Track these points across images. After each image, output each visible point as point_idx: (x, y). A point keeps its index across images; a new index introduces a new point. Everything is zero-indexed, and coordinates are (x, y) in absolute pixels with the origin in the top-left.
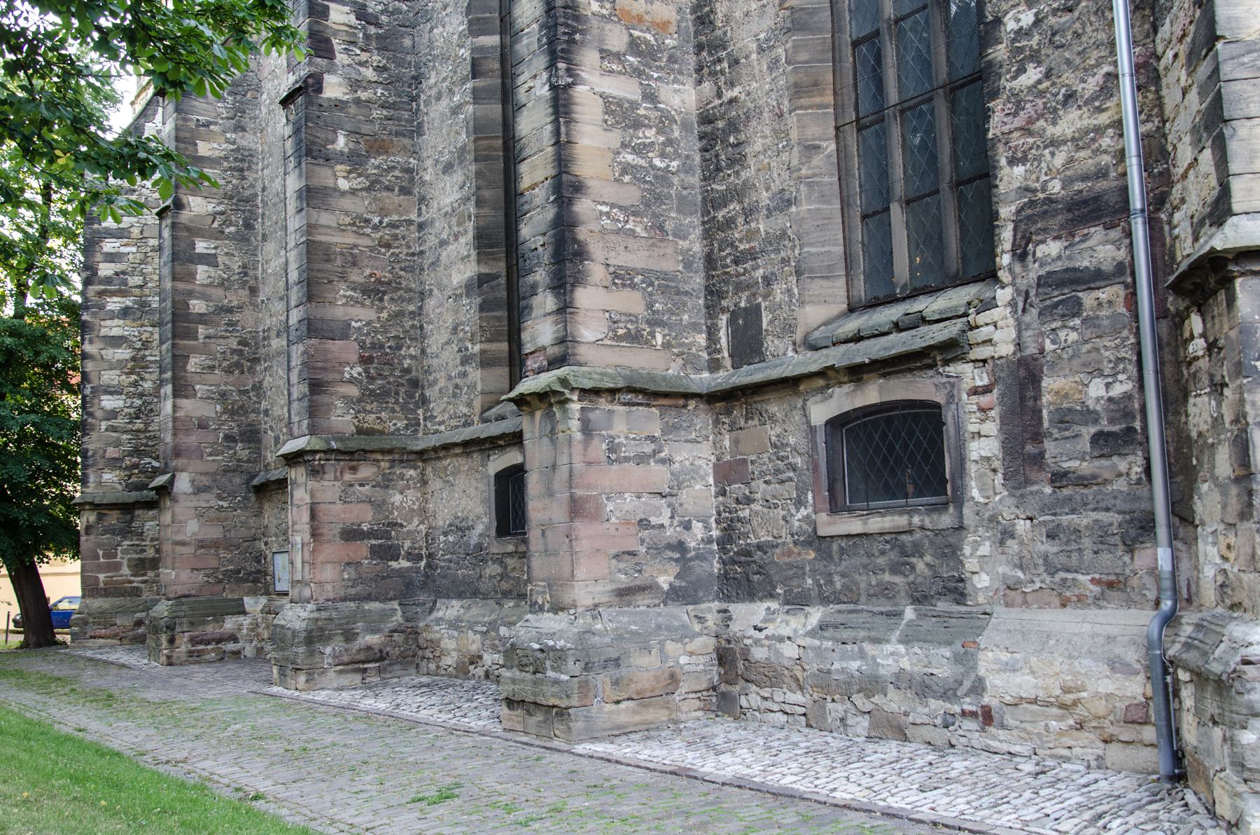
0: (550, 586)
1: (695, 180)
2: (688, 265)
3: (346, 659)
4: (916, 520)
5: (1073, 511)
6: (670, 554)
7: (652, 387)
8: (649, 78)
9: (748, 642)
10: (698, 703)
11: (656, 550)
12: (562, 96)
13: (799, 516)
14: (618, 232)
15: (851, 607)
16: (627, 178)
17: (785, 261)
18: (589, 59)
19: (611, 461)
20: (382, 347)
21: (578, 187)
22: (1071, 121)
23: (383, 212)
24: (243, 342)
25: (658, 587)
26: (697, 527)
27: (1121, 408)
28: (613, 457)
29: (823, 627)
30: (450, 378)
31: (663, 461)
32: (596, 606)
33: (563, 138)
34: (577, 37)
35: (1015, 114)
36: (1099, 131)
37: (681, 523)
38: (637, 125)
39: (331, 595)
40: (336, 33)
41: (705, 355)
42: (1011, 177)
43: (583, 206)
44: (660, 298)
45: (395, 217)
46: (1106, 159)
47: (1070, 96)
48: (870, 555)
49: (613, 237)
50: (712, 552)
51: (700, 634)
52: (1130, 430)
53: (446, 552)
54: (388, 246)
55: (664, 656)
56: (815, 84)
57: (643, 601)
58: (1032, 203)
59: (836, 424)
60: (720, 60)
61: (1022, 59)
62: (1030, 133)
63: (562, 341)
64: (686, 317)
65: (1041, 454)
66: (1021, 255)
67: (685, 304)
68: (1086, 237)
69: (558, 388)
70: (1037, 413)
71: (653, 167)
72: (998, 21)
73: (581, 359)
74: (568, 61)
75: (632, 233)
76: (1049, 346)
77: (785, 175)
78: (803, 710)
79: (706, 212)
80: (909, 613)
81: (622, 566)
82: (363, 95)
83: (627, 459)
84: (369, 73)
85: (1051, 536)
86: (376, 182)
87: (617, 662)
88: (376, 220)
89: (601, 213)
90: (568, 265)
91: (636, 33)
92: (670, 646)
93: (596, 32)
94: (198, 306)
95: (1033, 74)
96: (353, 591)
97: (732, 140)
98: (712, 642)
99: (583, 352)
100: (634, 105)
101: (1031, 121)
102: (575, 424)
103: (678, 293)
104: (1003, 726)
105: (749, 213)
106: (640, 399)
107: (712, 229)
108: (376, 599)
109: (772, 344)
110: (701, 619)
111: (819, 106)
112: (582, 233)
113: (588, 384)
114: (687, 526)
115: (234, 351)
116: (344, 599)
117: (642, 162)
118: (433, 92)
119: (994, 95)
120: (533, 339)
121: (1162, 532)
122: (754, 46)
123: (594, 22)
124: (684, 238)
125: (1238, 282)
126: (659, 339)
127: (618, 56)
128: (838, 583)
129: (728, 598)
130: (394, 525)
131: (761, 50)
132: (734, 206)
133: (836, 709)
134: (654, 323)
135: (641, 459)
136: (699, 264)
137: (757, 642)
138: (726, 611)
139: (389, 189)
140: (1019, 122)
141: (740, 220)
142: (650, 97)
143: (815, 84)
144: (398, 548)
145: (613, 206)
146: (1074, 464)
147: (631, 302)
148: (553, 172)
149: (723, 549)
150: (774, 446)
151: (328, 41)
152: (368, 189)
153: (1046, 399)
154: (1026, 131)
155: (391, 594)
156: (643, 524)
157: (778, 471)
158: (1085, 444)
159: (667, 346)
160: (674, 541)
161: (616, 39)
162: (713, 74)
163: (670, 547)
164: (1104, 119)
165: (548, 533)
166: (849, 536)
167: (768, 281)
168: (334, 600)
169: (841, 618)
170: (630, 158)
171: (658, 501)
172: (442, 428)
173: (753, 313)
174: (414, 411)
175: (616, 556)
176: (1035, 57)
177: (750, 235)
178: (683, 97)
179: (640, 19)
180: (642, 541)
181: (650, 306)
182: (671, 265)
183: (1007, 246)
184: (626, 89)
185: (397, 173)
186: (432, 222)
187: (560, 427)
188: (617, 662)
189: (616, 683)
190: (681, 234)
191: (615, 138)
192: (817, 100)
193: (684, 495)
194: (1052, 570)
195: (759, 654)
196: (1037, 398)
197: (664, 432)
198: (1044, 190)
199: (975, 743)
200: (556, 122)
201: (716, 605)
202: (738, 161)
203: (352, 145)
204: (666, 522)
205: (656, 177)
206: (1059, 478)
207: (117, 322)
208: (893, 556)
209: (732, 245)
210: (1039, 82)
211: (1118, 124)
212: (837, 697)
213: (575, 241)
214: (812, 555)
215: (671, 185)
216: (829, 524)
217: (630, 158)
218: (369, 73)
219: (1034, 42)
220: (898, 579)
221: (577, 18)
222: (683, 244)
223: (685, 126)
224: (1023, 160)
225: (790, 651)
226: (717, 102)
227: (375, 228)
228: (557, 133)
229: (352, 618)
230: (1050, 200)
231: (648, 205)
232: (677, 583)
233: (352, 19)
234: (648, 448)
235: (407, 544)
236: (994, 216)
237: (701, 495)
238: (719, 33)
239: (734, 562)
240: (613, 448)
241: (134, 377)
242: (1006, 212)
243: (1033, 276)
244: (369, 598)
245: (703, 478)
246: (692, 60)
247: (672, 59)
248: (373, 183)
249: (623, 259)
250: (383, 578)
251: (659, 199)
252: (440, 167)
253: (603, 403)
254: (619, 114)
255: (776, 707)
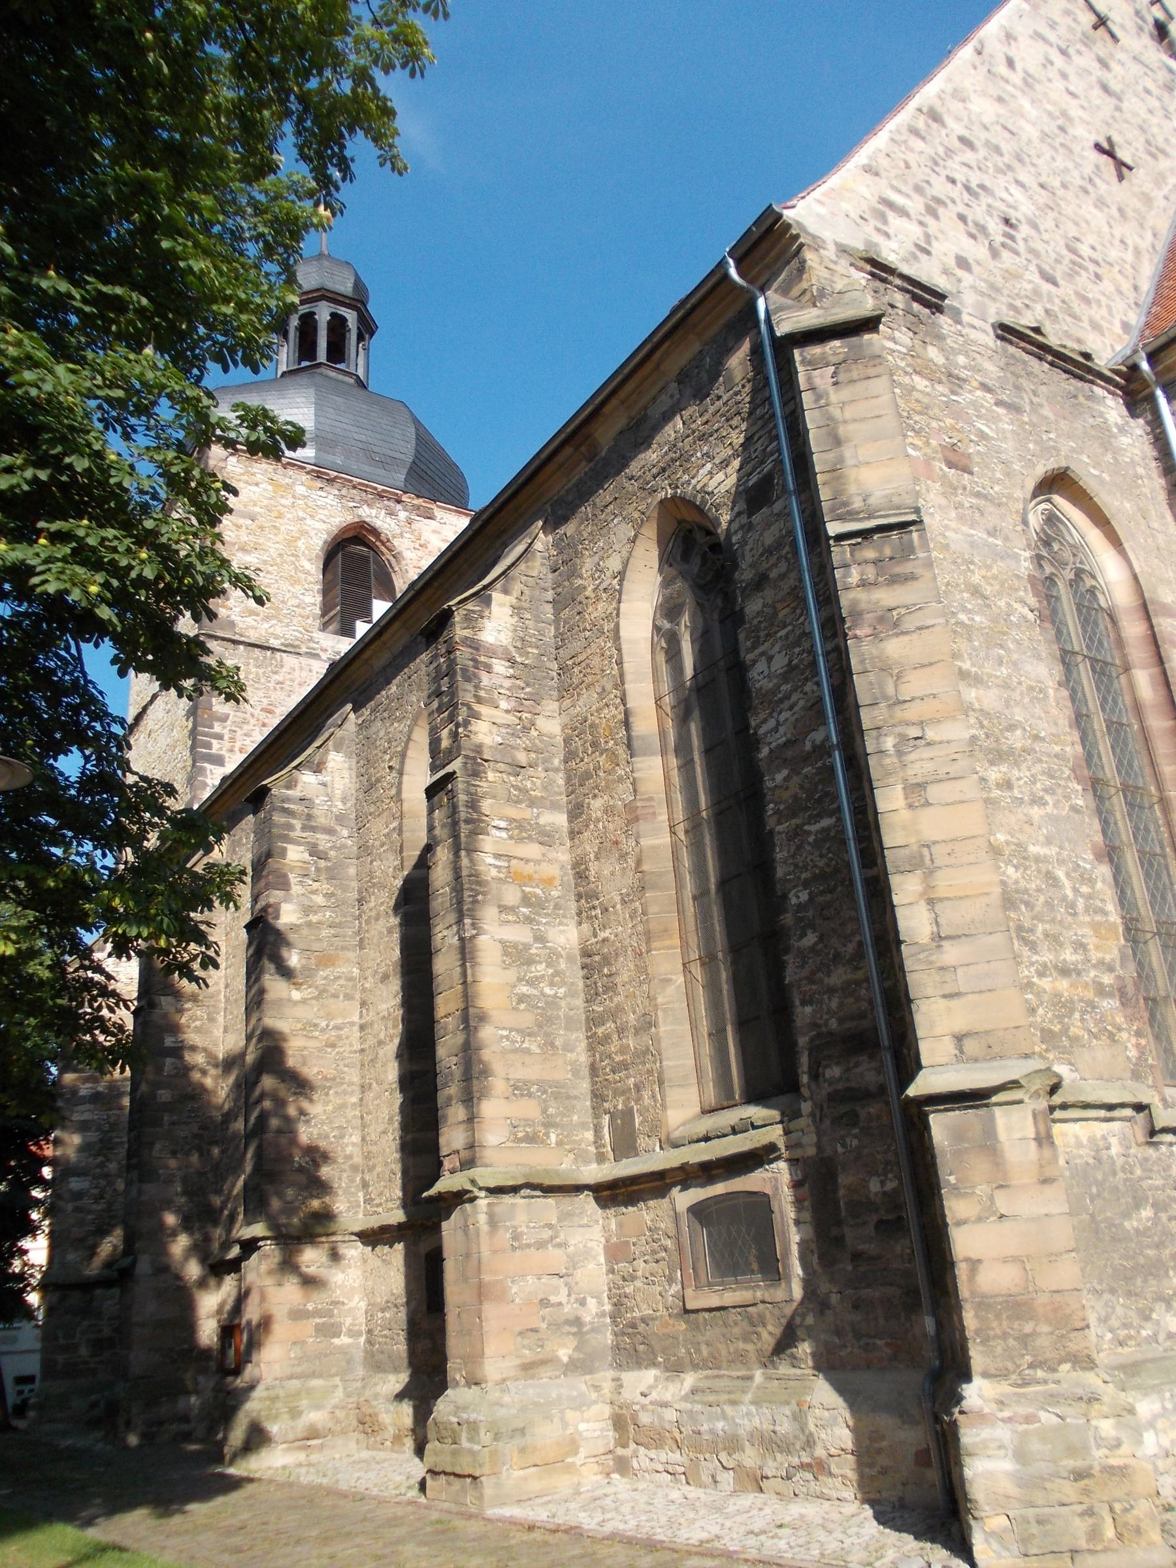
0: (465, 1364)
1: (579, 1002)
2: (576, 1073)
3: (291, 1437)
4: (759, 1294)
5: (868, 1286)
6: (567, 1328)
7: (547, 1182)
8: (538, 923)
9: (636, 1407)
10: (596, 1467)
11: (555, 1326)
12: (468, 945)
13: (672, 1292)
14: (516, 1051)
15: (715, 1372)
16: (522, 1006)
17: (650, 1072)
18: (489, 915)
19: (514, 1248)
20: (327, 1137)
21: (483, 1018)
22: (838, 976)
23: (329, 1016)
24: (203, 1127)
25: (558, 1359)
26: (592, 1303)
27: (892, 1199)
28: (516, 1244)
29: (693, 1392)
30: (386, 1164)
31: (559, 1245)
32: (504, 1380)
33: (469, 979)
34: (480, 897)
35: (802, 967)
36: (858, 983)
37: (577, 1300)
38: (530, 962)
39: (279, 1375)
40: (292, 869)
41: (592, 1149)
42: (804, 1013)
43: (486, 1033)
44: (552, 1103)
45: (340, 1021)
46: (864, 1005)
47: (837, 957)
48: (726, 1325)
49: (512, 1056)
50: (605, 1325)
51: (595, 1402)
52: (900, 1218)
53: (383, 1328)
54: (333, 1046)
55: (565, 1424)
56: (666, 931)
57: (545, 1373)
58: (819, 1035)
59: (697, 1211)
60: (594, 908)
61: (805, 926)
62: (813, 982)
63: (471, 1146)
64: (575, 1118)
65: (843, 1237)
66: (815, 1076)
67: (574, 1107)
68: (857, 1065)
69: (468, 1187)
70: (836, 1202)
71: (544, 995)
72: (785, 897)
73: (486, 1161)
74: (473, 918)
75: (527, 1051)
76: (840, 1149)
77: (647, 1002)
78: (682, 1469)
79: (589, 1029)
80: (758, 1375)
81: (526, 1342)
82: (314, 918)
83: (529, 1246)
84: (319, 900)
85: (856, 1307)
86: (325, 991)
87: (522, 1431)
88: (324, 1024)
89: (502, 1037)
90: (475, 1082)
91: (527, 889)
92: (570, 1415)
93: (494, 892)
94: (164, 1095)
95: (810, 939)
96: (298, 1370)
97: (606, 971)
98: (607, 1410)
99: (488, 1155)
100: (527, 947)
101: (813, 973)
102: (482, 1218)
103: (568, 1097)
104: (831, 1474)
105: (621, 1031)
106: (538, 1193)
107: (595, 1043)
108: (320, 1376)
109: (642, 1142)
110: (597, 1388)
111: (670, 948)
112: (486, 1054)
113: (492, 1184)
114: (583, 1303)
115: (196, 1136)
116: (291, 1377)
117: (535, 992)
118: (373, 914)
119: (787, 951)
120: (448, 1144)
121: (925, 1301)
122: (618, 899)
123: (494, 885)
124: (572, 1051)
125: (931, 1117)
126: (553, 1137)
127: (512, 909)
128: (705, 1351)
129: (620, 1367)
130: (336, 1303)
131: (624, 902)
132: (610, 1025)
133: (709, 1466)
134: (548, 1125)
135: (541, 1245)
136: (585, 1072)
137: (643, 1407)
138: (618, 1379)
139: (335, 996)
140: (805, 972)
141: (615, 1036)
142: (540, 938)
143: (666, 931)
144: (340, 1325)
145: (511, 1030)
146: (866, 1246)
147: (529, 1109)
148: (462, 1006)
149: (614, 1322)
150: (650, 1230)
151: (285, 876)
152: (316, 998)
153: (842, 1192)
154: (811, 980)
155: (334, 1370)
156: (544, 1303)
157: (654, 1252)
158: (870, 1230)
159: (560, 1144)
160: (571, 1317)
161: (511, 896)
162: (589, 918)
163: (568, 1322)
164: (860, 975)
165: (464, 1316)
166: (710, 1310)
167: (638, 1088)
168: (281, 1379)
169: (708, 1383)
170: (524, 989)
171: (556, 1281)
172: (380, 1210)
173: (628, 1114)
174: (355, 1194)
175: (521, 1333)
176: (812, 926)
177: (623, 1050)
178: (567, 936)
179: (530, 878)
180: (544, 1319)
181: (544, 1111)
182: (561, 1074)
183: (805, 1068)
184: (520, 934)
185: (342, 982)
186: (372, 1024)
187: (470, 1221)
188: (522, 1431)
189: (522, 1450)
190: (568, 1048)
191: (511, 975)
192: (667, 943)
193: (578, 1274)
194: (858, 1336)
195: (645, 1419)
196: (835, 1191)
197: (560, 1220)
198: (826, 1025)
199: (811, 1491)
200: (463, 966)
201: (611, 1374)
202: (611, 988)
203: (304, 962)
204: (564, 1299)
205: (546, 1003)
206: (856, 1257)
207: (88, 1106)
208: (745, 1324)
209: (610, 1057)
210: (816, 944)
211: (867, 980)
212: (707, 1456)
213: (480, 1061)
214: (684, 1326)
215: (559, 1008)
216: (695, 1298)
217: (524, 989)
218: (319, 900)
219: (810, 914)
220: (750, 1347)
221: (479, 883)
222: (570, 1056)
223: (570, 959)
224: (810, 1003)
225: (670, 1415)
226: (594, 940)
227: (323, 1031)
228: (464, 974)
229: (297, 1395)
230: (831, 1034)
231: (540, 1026)
232: (576, 1355)
233: (306, 856)
234: (546, 1234)
235: (349, 1321)
236: (795, 1043)
237: (594, 1273)
238: (592, 886)
239: (623, 1334)
240: (516, 1237)
241: (100, 1159)
242: (802, 1041)
243: (824, 1092)
244: (313, 1375)
245: (595, 1258)
246: (573, 906)
247: (557, 907)
248: (321, 993)
249: (519, 1073)
250: (326, 1355)
251: (550, 1021)
252: (378, 977)
253: (507, 1199)
254: (516, 955)
255: (660, 1468)
